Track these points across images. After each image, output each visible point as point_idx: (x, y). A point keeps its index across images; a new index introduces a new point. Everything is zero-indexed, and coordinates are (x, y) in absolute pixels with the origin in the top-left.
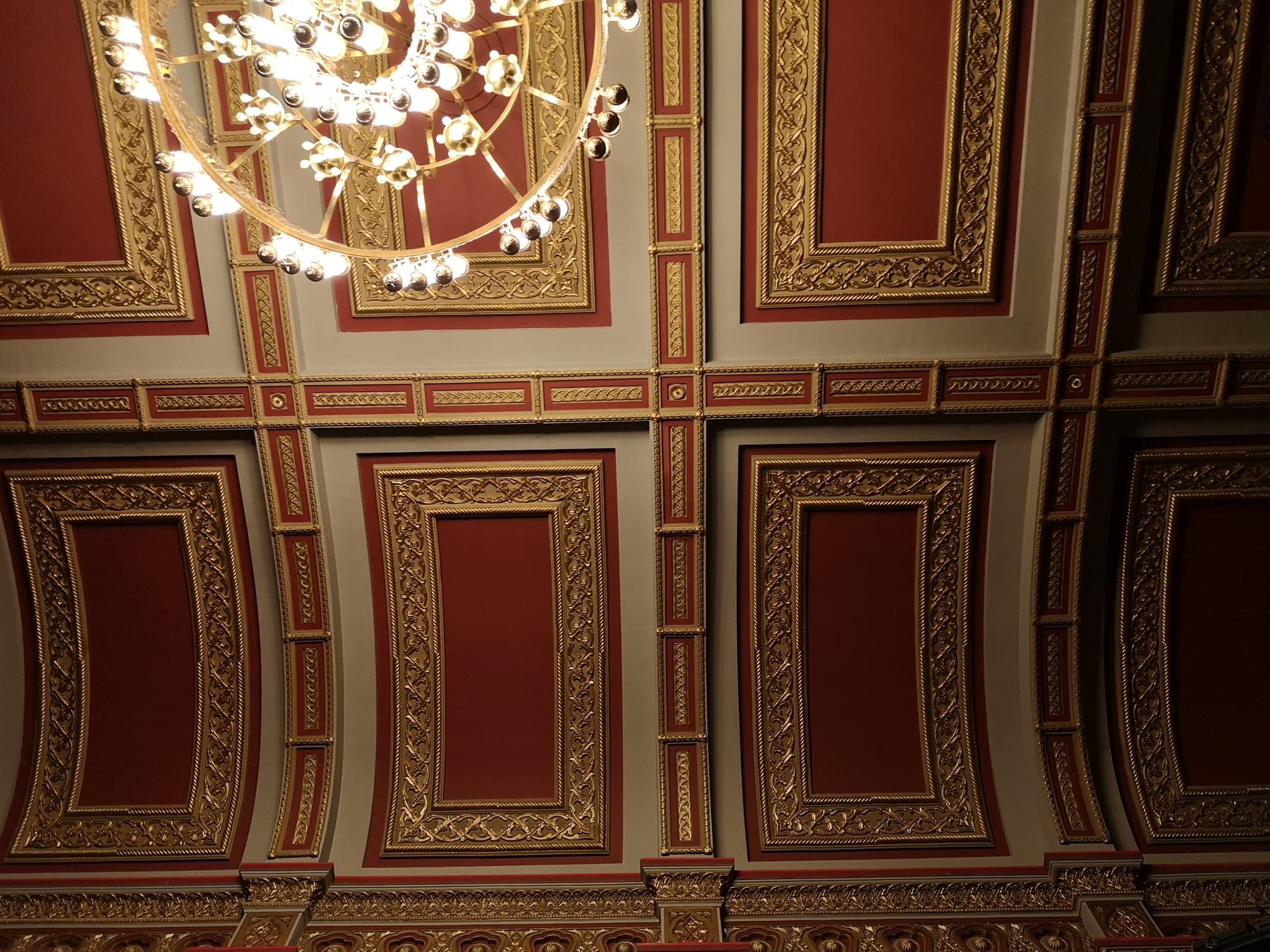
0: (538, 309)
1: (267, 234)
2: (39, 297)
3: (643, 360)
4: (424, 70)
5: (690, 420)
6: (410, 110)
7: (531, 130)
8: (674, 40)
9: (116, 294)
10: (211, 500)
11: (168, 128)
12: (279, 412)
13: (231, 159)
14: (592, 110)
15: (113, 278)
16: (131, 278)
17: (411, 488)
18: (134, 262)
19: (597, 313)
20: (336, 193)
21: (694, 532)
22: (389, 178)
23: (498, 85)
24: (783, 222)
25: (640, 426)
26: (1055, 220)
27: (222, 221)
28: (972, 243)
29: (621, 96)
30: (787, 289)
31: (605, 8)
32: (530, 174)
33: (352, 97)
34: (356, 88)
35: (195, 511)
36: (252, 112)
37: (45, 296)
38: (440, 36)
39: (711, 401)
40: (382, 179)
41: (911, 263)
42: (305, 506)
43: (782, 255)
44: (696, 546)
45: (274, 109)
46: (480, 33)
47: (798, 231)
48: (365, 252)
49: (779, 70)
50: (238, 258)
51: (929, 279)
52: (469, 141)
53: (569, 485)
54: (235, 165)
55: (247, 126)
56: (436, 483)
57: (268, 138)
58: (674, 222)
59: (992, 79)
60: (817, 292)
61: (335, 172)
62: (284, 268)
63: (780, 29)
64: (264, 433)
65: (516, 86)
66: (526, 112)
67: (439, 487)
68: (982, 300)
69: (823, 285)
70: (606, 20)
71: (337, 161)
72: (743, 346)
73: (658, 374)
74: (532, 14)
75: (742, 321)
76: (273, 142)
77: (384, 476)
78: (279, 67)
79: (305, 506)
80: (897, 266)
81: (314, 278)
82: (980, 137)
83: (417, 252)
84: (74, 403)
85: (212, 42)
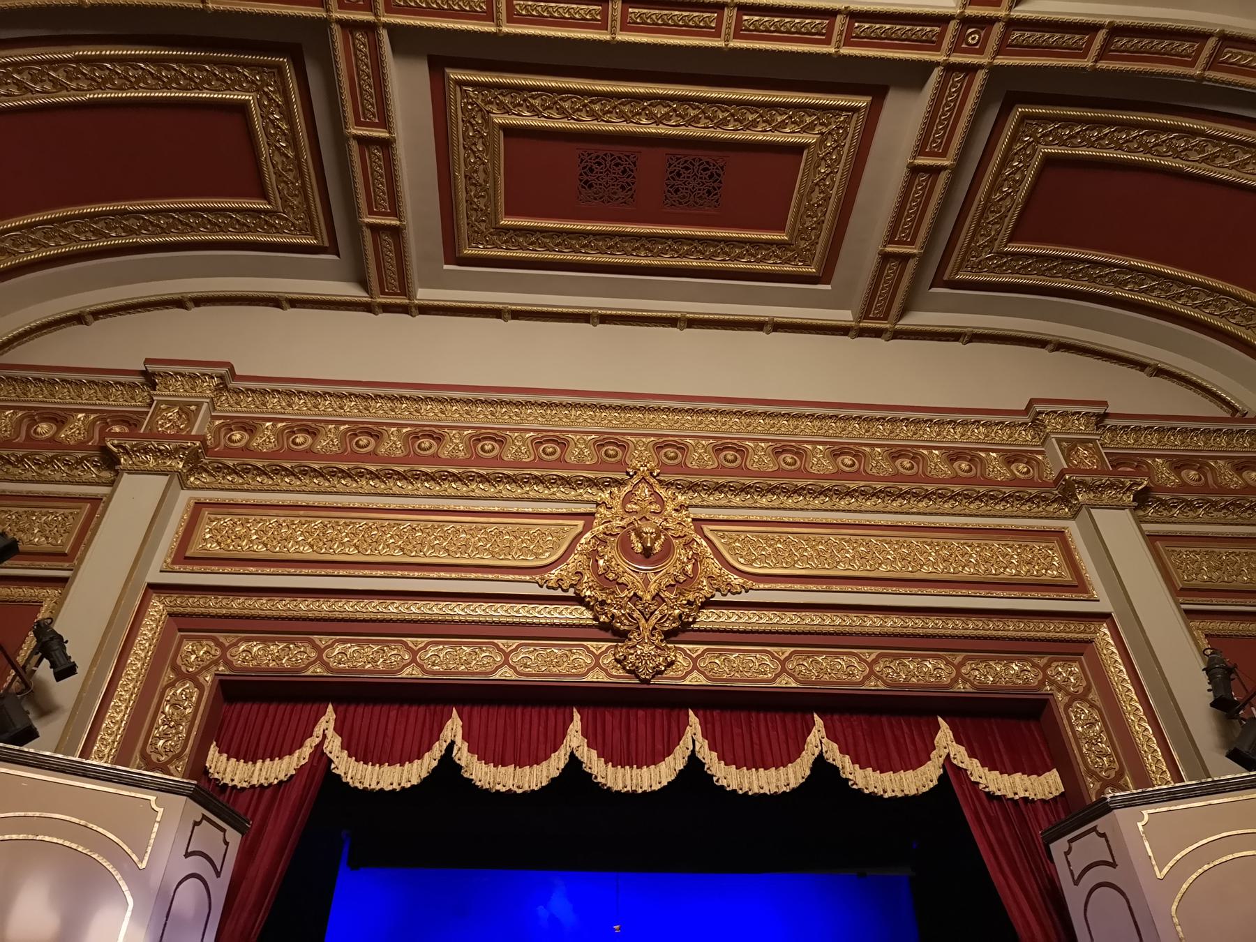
70: (153, 798)
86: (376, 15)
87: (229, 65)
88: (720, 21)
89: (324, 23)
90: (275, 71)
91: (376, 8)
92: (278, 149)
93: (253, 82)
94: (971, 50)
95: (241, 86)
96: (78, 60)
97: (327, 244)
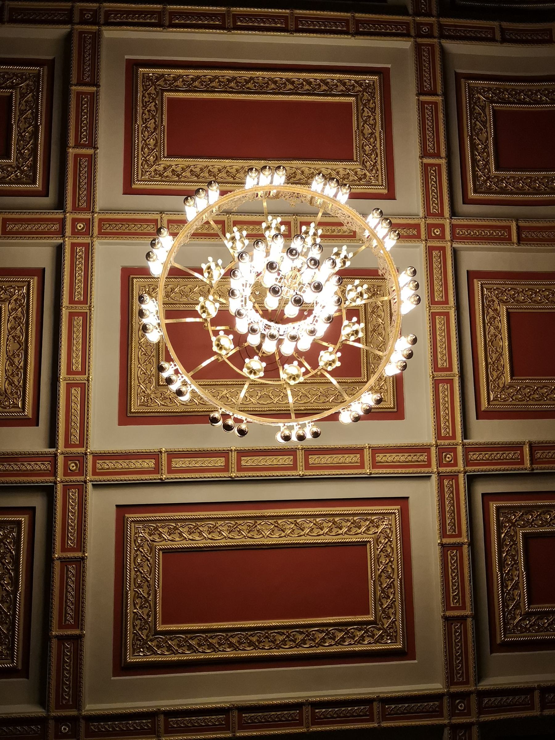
0: (131, 382)
1: (174, 235)
2: (148, 108)
3: (97, 443)
4: (256, 327)
5: (55, 474)
6: (237, 318)
7: (230, 383)
8: (275, 462)
9: (148, 149)
10: (21, 179)
11: (231, 192)
12: (74, 226)
13: (216, 222)
14: (235, 416)
15: (157, 149)
16: (157, 158)
17: (20, 298)
18: (165, 162)
19: (126, 417)
20: (196, 275)
21: (56, 477)
22: (202, 303)
23: (249, 365)
24: (176, 528)
25: (52, 442)
26: (168, 699)
27: (182, 212)
28: (159, 647)
29: (242, 433)
30: (136, 533)
31: (286, 424)
32: (203, 382)
33: (244, 288)
34: (248, 291)
35: (14, 168)
36: (237, 235)
37: (149, 111)
38: (272, 337)
39: (67, 488)
40: (201, 299)
41: (148, 609)
42: (11, 233)
43: (156, 529)
44: (47, 478)
45: (239, 247)
46: (277, 358)
47: (170, 538)
48: (162, 284)
49: (259, 522)
50: (166, 217)
51: (138, 622)
52: (221, 349)
53: (15, 396)
54: (212, 223)
55: (232, 232)
56: (22, 313)
57: (226, 242)
58: (178, 463)
59: (252, 648)
60: (133, 551)
61: (206, 274)
62: (154, 240)
63: (279, 522)
64: (61, 216)
65: (248, 375)
66: (240, 381)
67: (19, 315)
68: (123, 658)
69: (137, 555)
70: (281, 425)
71: (212, 277)
72: (101, 507)
73: (86, 454)
74: (285, 386)
75: (117, 506)
76: (224, 245)
77: (29, 282)
78: (259, 251)
79: (11, 233)
80: (147, 601)
81: (148, 256)
82: (220, 644)
83: (162, 315)
84: (86, 113)
85: (272, 220)
88: (301, 714)
94: (462, 714)
97: (463, 80)
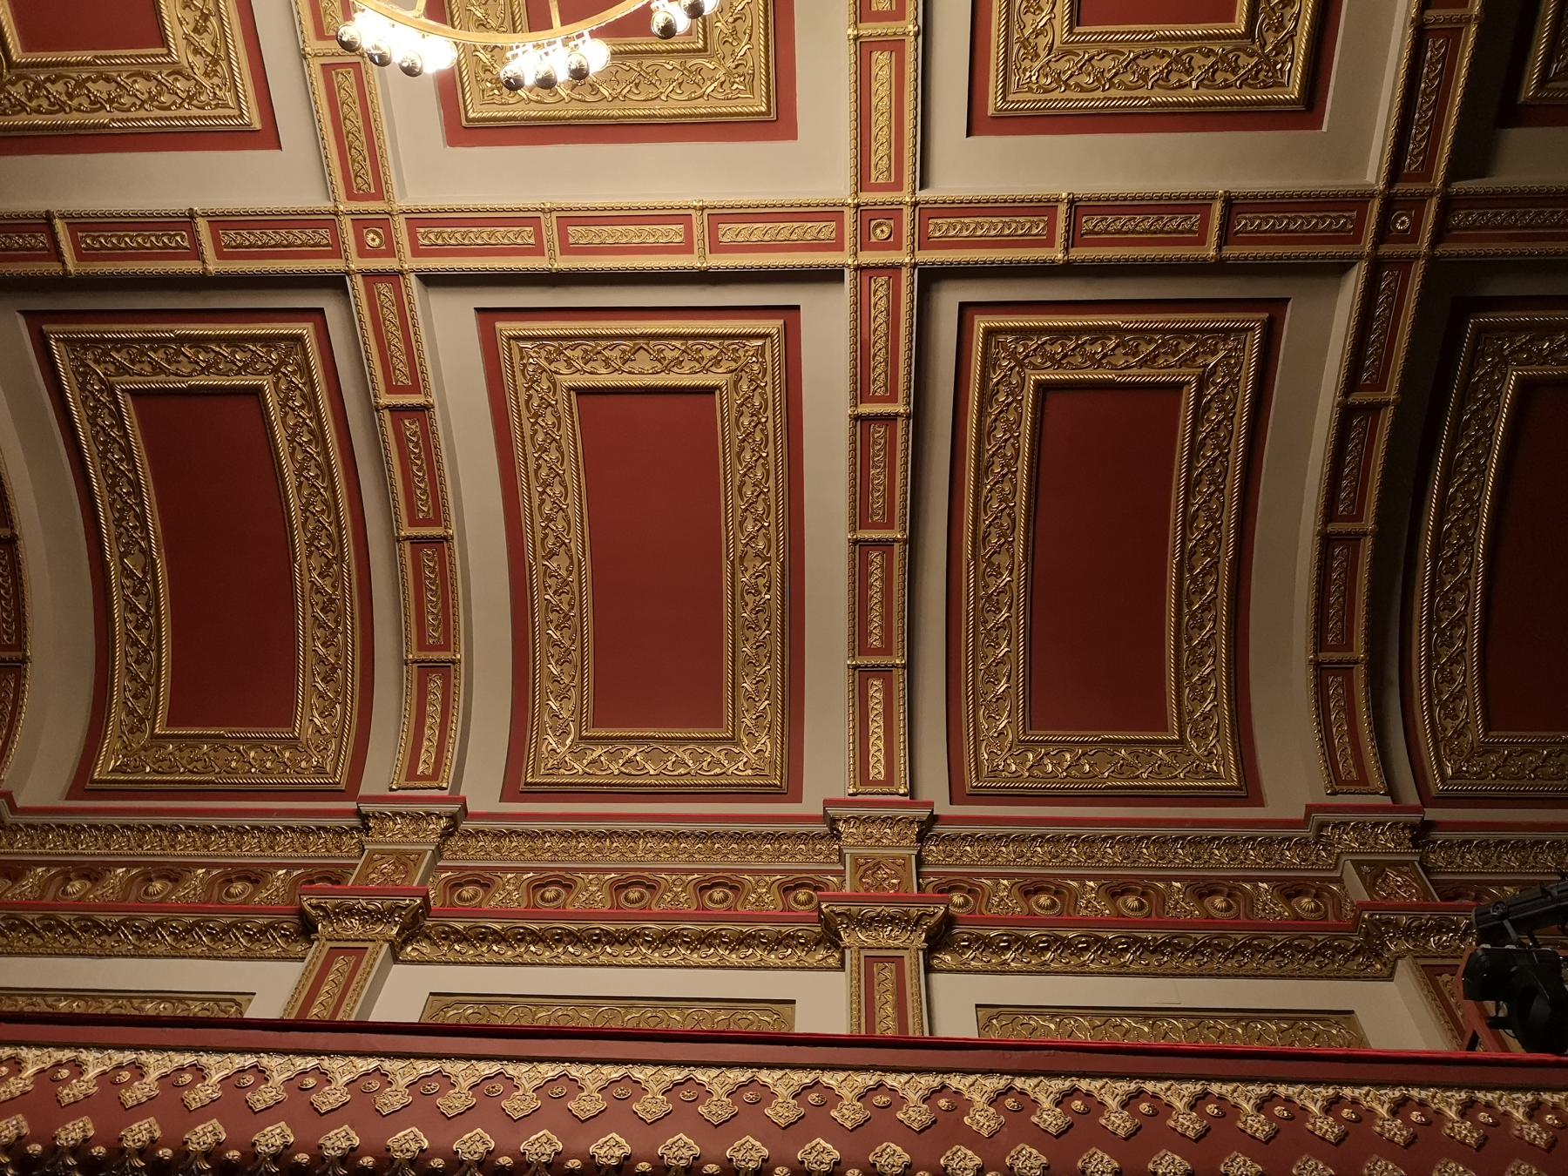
86: (1431, 195)
87: (1467, 394)
89: (1433, 262)
90: (1483, 336)
91: (1422, 194)
92: (1552, 352)
93: (1494, 366)
95: (1497, 382)
96: (1435, 556)
